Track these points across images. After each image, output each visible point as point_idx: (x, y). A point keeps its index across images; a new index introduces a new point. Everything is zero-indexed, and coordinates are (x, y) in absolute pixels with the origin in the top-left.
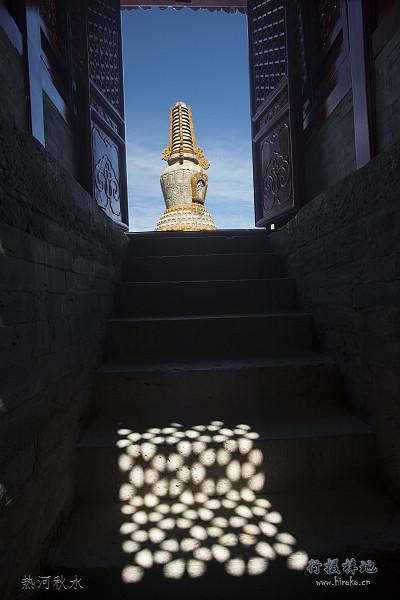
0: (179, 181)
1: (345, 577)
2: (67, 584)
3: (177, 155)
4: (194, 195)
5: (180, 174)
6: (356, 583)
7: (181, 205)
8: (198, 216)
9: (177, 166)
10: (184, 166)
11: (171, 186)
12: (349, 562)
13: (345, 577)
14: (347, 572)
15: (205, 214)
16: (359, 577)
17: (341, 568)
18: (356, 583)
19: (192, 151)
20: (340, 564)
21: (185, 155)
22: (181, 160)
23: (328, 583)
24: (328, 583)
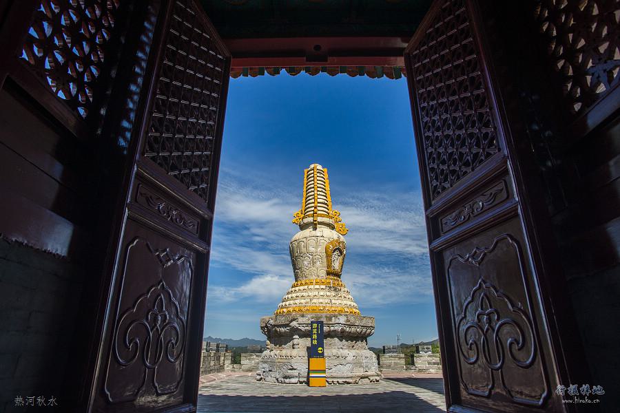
0: (312, 249)
1: (582, 397)
2: (46, 402)
3: (311, 219)
4: (329, 266)
5: (312, 242)
6: (590, 402)
7: (313, 278)
8: (333, 293)
9: (308, 232)
10: (318, 232)
11: (301, 255)
12: (585, 387)
13: (582, 397)
14: (584, 394)
15: (343, 289)
16: (592, 397)
17: (579, 391)
18: (590, 402)
19: (328, 215)
20: (578, 388)
21: (319, 219)
22: (314, 225)
23: (571, 401)
24: (571, 401)
